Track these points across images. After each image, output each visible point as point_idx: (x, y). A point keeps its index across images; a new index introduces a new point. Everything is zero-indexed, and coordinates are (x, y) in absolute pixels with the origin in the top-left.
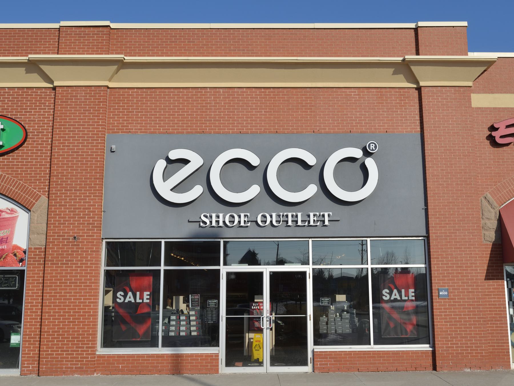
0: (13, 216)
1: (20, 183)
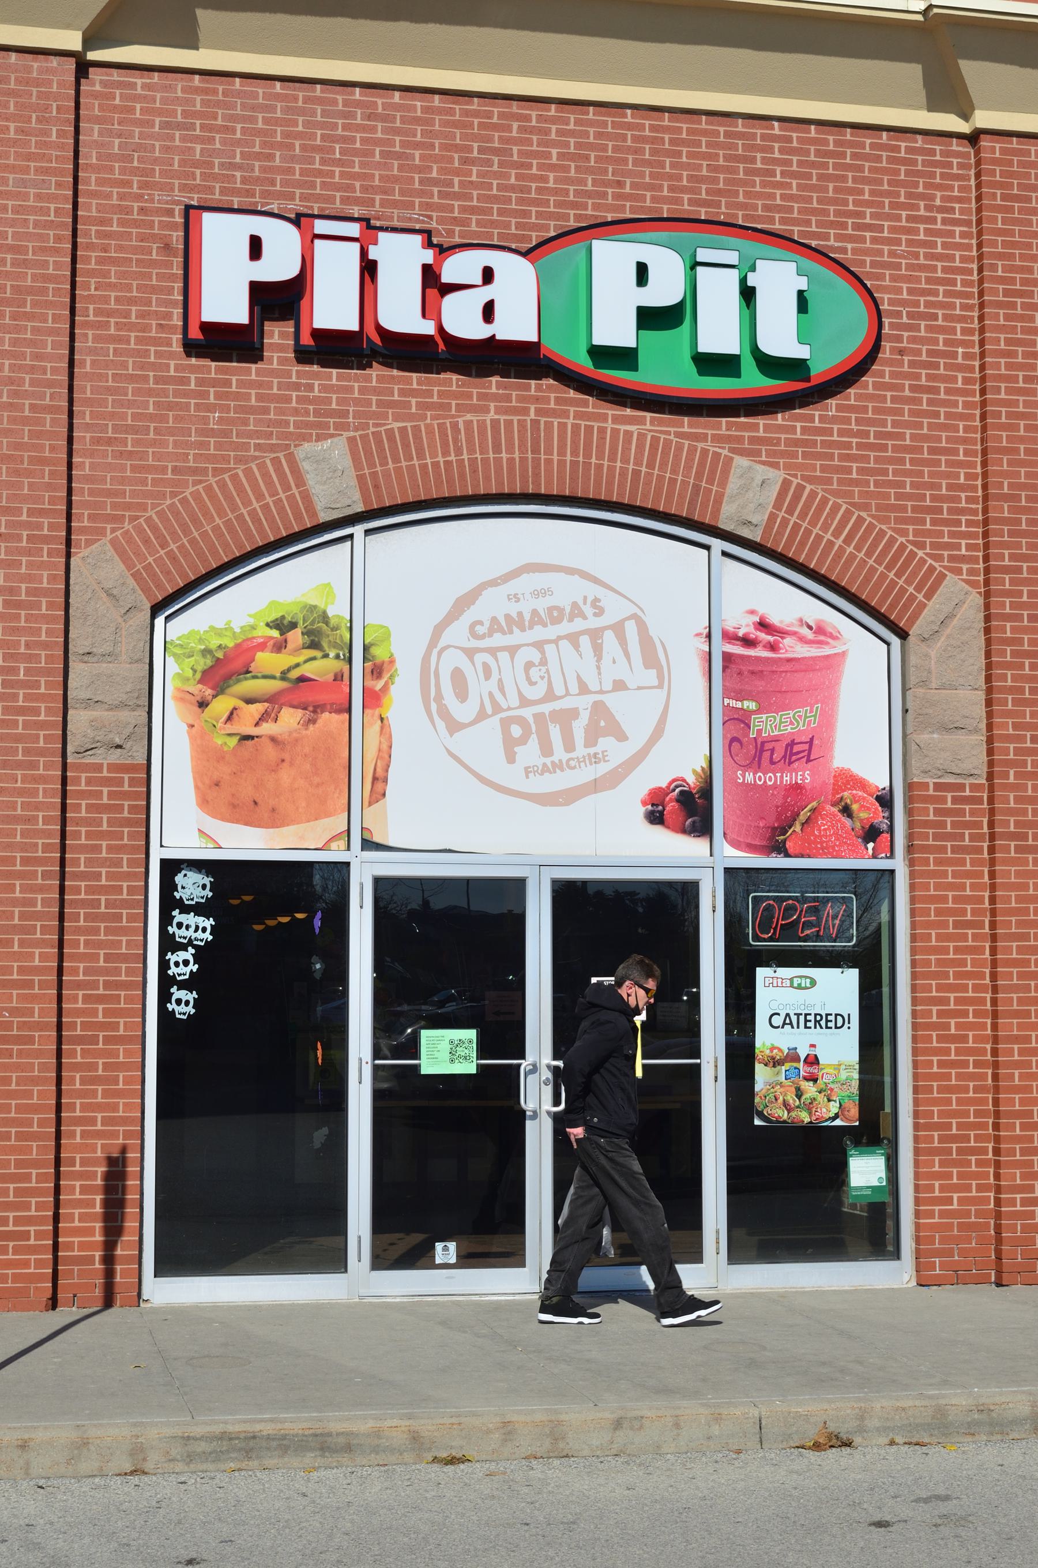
0: (827, 651)
1: (860, 520)
